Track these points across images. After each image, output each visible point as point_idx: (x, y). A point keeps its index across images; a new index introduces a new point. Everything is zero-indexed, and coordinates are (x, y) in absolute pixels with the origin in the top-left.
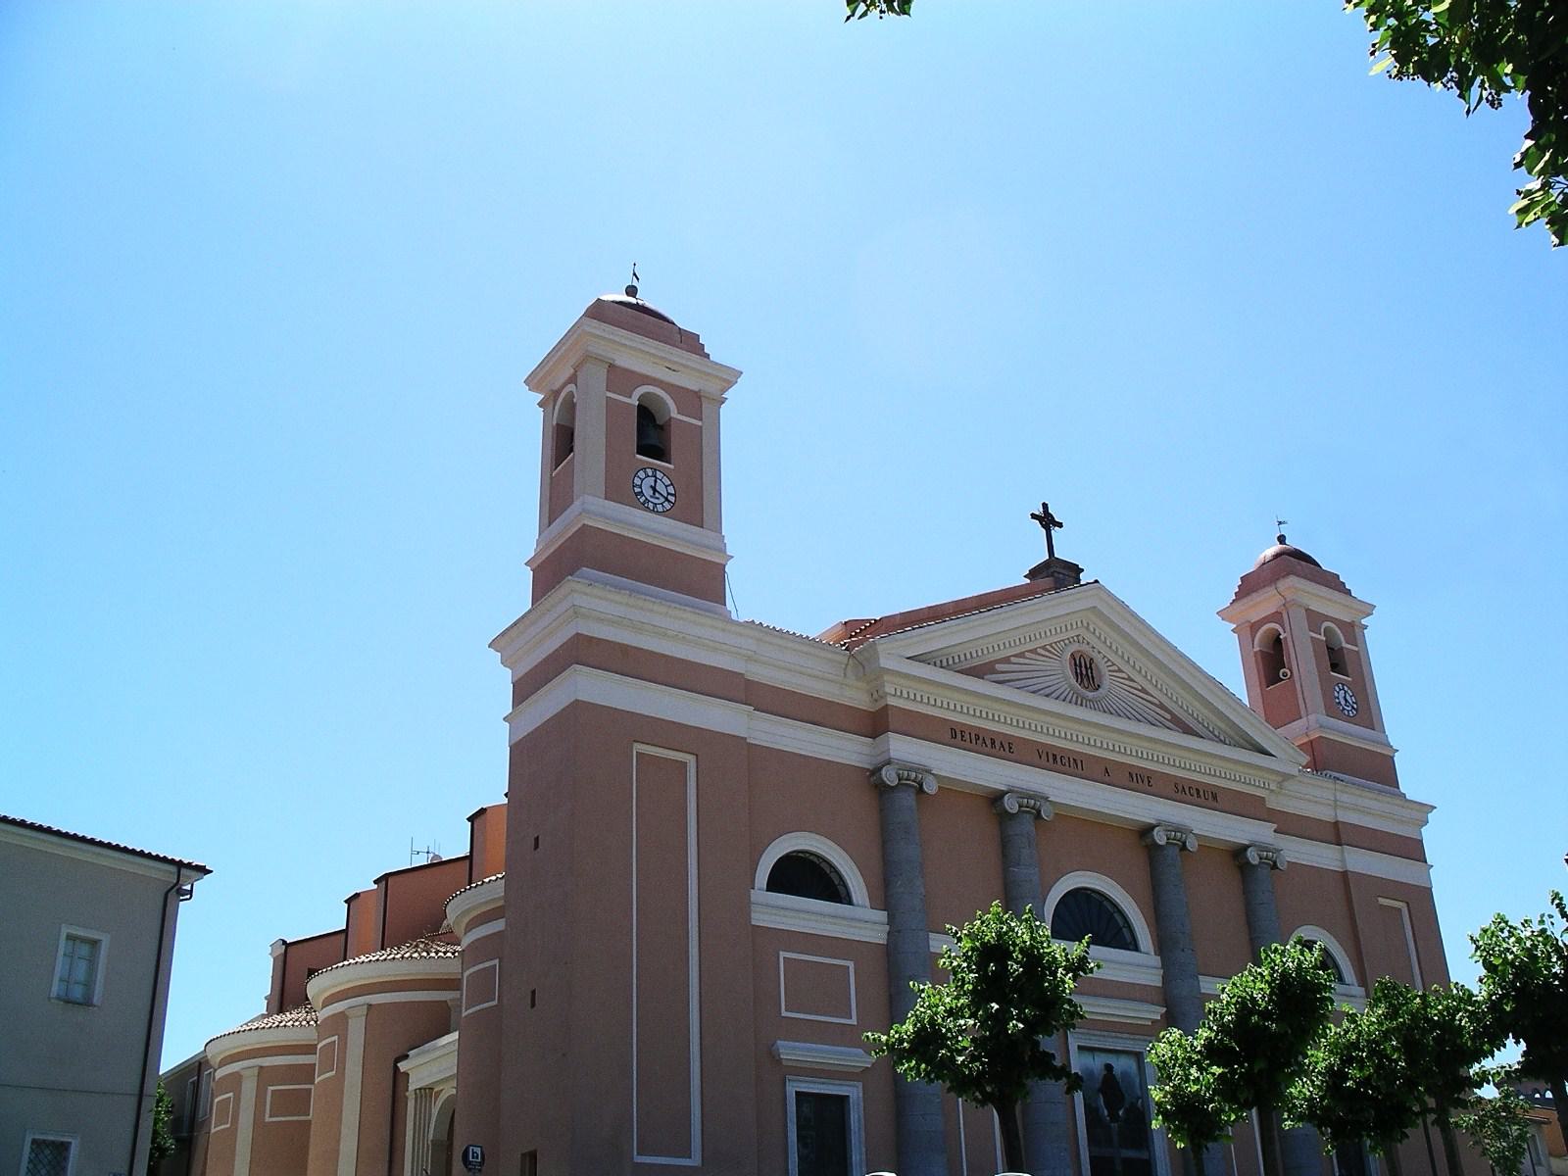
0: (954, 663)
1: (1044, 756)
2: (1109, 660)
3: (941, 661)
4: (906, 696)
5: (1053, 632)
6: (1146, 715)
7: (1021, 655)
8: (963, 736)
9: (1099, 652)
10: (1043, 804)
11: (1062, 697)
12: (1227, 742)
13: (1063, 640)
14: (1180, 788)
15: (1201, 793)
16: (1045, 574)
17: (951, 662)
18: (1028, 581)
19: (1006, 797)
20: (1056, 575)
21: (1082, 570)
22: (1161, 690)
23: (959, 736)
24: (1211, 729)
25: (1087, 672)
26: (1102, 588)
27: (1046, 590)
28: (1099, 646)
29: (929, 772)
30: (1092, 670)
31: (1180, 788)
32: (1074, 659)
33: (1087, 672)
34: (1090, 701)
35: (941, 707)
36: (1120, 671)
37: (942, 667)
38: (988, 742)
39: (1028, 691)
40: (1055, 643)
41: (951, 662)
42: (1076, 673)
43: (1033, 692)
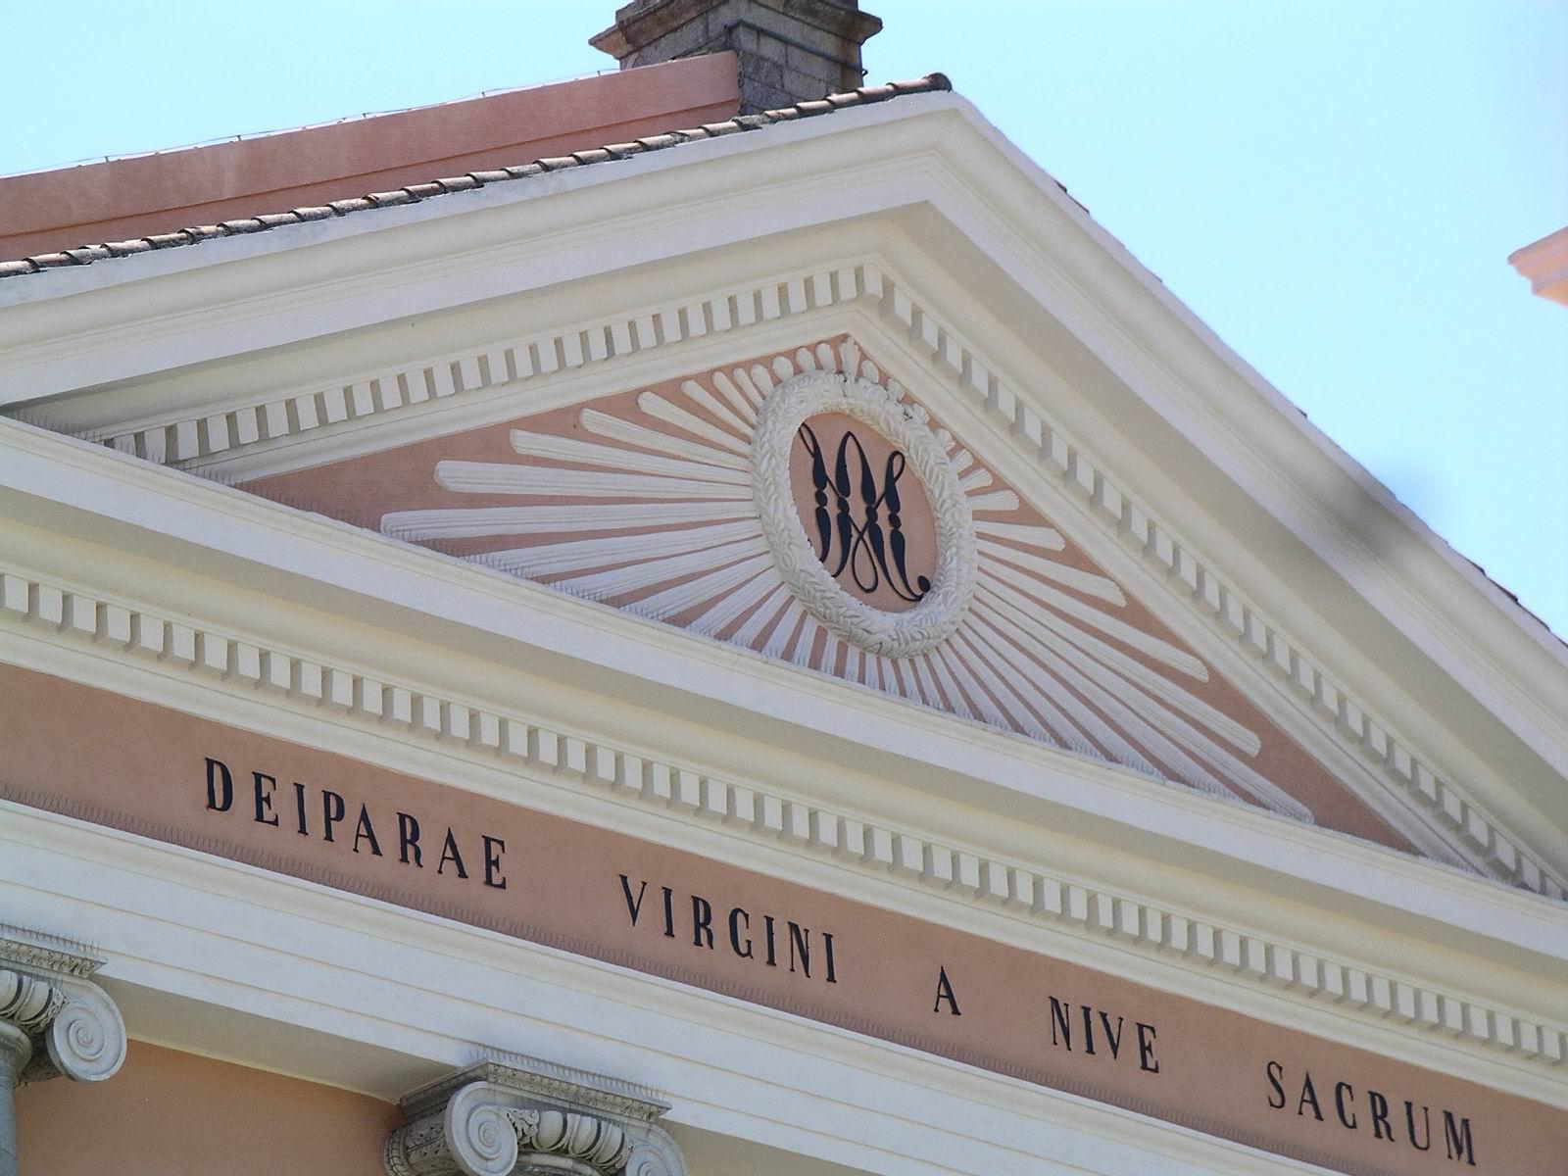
0: (235, 443)
1: (651, 909)
2: (978, 464)
3: (171, 432)
4: (1484, 1033)
5: (722, 319)
6: (1138, 729)
7: (564, 422)
8: (261, 800)
9: (935, 425)
10: (632, 1134)
11: (751, 629)
12: (1531, 875)
13: (767, 361)
14: (1294, 1091)
15: (1396, 1116)
16: (692, 34)
17: (219, 439)
18: (607, 64)
19: (460, 1103)
20: (747, 41)
21: (874, 25)
22: (1220, 615)
23: (244, 795)
24: (1429, 789)
25: (871, 513)
26: (968, 120)
27: (700, 114)
28: (937, 394)
29: (84, 968)
30: (894, 504)
31: (1294, 1091)
32: (817, 454)
33: (871, 513)
34: (880, 651)
35: (129, 647)
36: (1027, 515)
37: (172, 461)
38: (388, 835)
39: (642, 614)
40: (729, 370)
41: (219, 439)
42: (822, 517)
43: (617, 602)
